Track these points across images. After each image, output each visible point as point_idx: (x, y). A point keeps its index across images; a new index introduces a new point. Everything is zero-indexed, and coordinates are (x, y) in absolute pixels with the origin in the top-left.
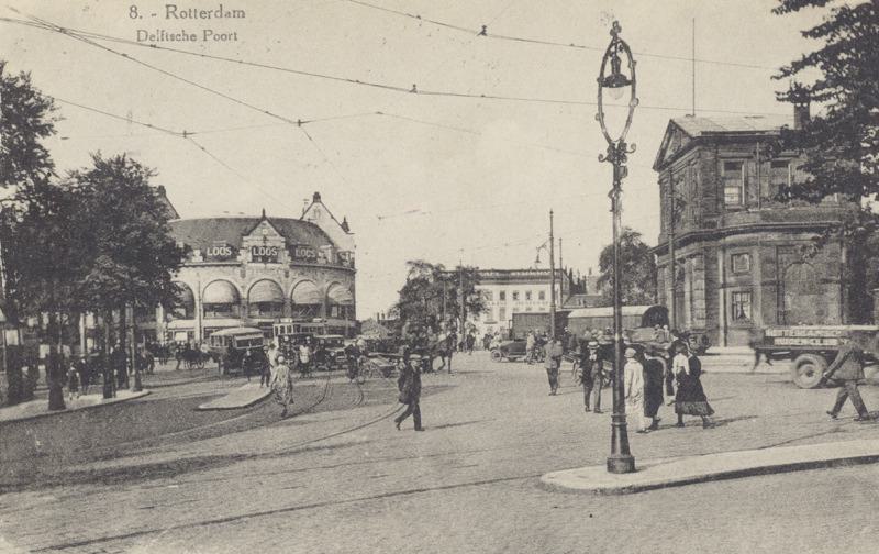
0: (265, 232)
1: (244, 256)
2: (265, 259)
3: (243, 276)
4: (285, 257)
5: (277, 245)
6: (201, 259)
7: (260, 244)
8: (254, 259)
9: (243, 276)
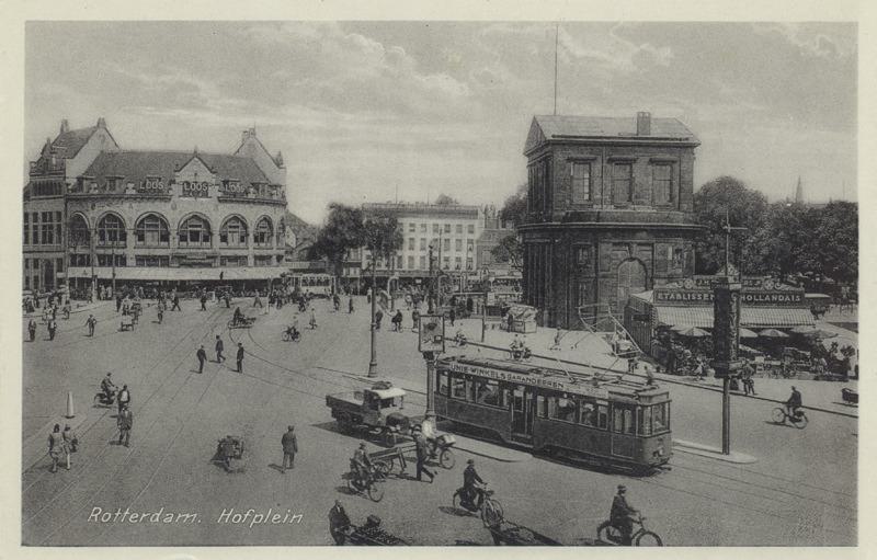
0: (195, 168)
1: (176, 190)
2: (196, 194)
3: (174, 208)
4: (215, 192)
6: (134, 192)
7: (191, 179)
9: (174, 208)
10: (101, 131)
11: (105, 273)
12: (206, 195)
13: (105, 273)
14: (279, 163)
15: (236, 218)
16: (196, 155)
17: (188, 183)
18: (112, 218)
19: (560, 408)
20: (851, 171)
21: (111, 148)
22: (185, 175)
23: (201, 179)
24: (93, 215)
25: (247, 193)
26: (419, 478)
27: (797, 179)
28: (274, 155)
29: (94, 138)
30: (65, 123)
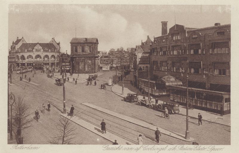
1: (34, 50)
3: (34, 54)
4: (42, 50)
5: (41, 48)
8: (36, 51)
9: (34, 54)
10: (22, 39)
11: (152, 51)
12: (40, 51)
13: (152, 51)
14: (59, 44)
15: (30, 56)
16: (38, 43)
17: (37, 49)
18: (23, 56)
19: (194, 73)
20: (230, 22)
21: (25, 42)
22: (36, 48)
23: (39, 48)
24: (20, 55)
25: (49, 50)
26: (90, 85)
27: (202, 124)
28: (58, 42)
29: (22, 40)
30: (18, 38)
